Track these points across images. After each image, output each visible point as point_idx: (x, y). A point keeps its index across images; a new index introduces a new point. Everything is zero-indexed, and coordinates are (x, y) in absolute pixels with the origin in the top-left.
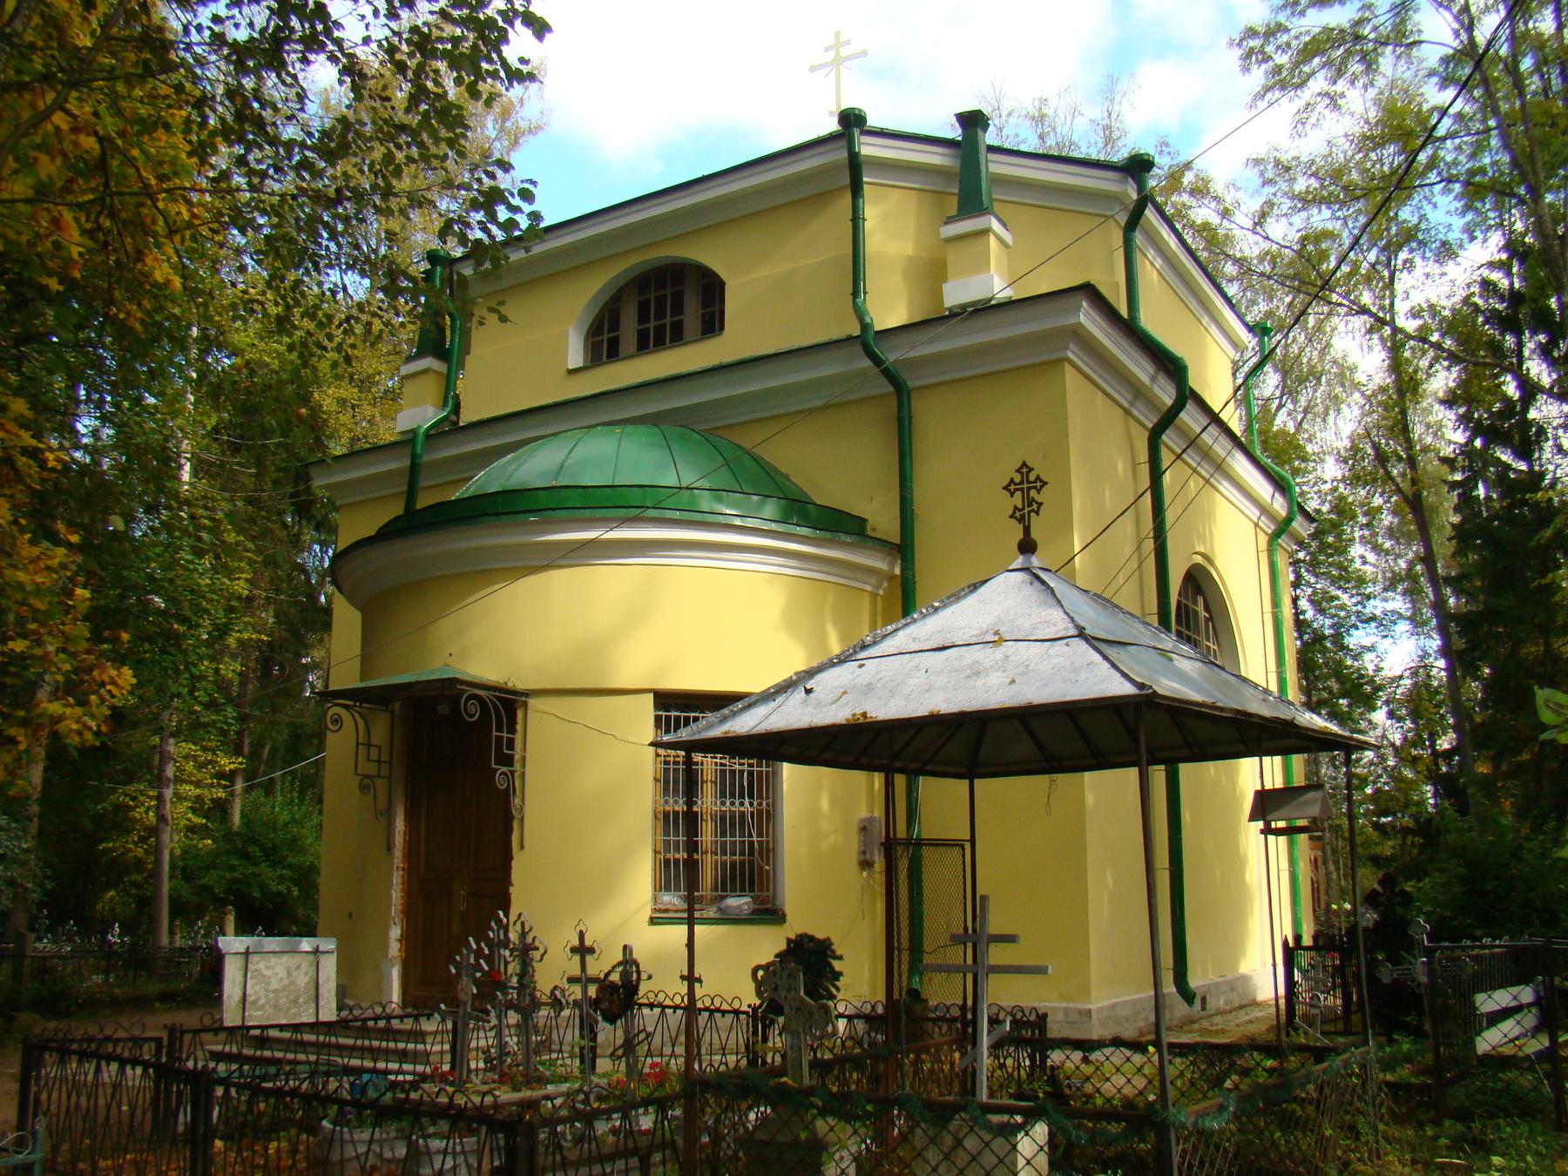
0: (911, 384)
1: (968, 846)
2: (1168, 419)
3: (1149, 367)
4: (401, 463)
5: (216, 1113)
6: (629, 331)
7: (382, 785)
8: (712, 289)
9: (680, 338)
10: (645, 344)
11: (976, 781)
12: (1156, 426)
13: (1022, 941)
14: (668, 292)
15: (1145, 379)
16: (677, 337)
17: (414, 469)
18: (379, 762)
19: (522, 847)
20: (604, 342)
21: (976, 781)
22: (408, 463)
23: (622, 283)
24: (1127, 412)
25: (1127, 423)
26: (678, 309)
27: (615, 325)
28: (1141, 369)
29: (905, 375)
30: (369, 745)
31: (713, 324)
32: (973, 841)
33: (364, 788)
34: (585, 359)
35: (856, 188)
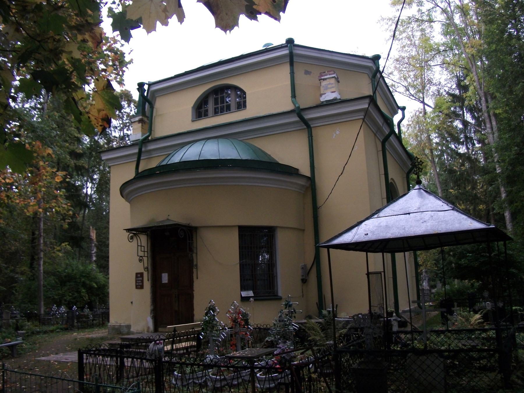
0: (312, 126)
1: (383, 273)
3: (382, 121)
4: (136, 150)
6: (211, 106)
7: (145, 259)
9: (230, 110)
10: (217, 112)
11: (368, 253)
12: (383, 140)
15: (381, 124)
18: (144, 251)
19: (197, 278)
21: (385, 254)
24: (375, 135)
25: (375, 139)
28: (380, 121)
29: (310, 123)
30: (141, 246)
31: (242, 105)
32: (384, 272)
33: (140, 260)
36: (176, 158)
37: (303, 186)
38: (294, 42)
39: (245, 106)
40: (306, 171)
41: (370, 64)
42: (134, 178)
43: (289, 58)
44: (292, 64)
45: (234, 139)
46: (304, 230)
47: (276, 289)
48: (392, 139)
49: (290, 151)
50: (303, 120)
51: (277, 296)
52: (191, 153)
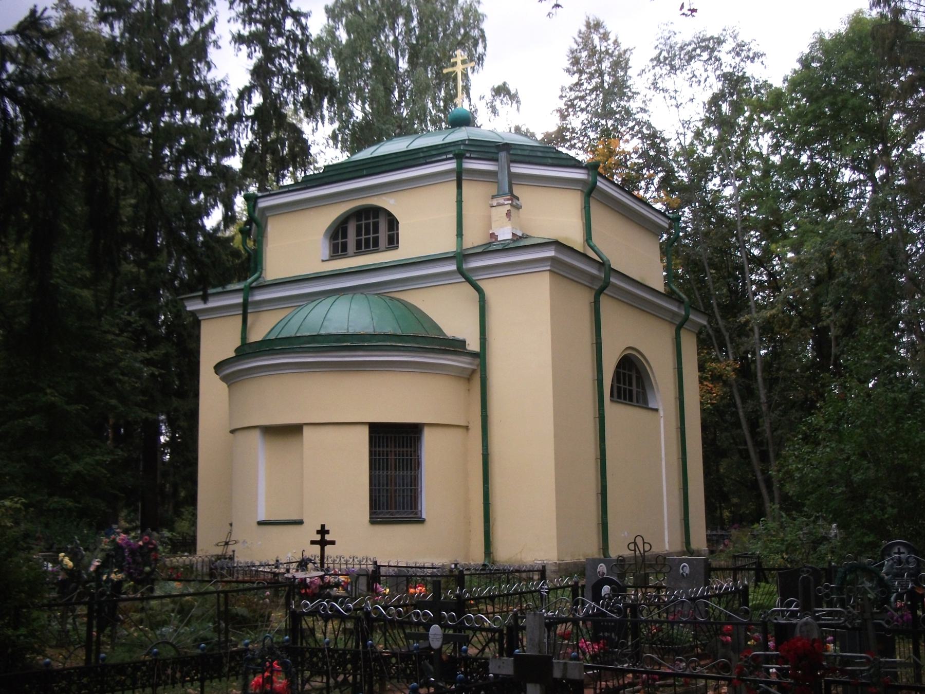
8: (393, 223)
17: (245, 306)
26: (376, 230)
27: (345, 235)
31: (393, 242)
43: (455, 175)
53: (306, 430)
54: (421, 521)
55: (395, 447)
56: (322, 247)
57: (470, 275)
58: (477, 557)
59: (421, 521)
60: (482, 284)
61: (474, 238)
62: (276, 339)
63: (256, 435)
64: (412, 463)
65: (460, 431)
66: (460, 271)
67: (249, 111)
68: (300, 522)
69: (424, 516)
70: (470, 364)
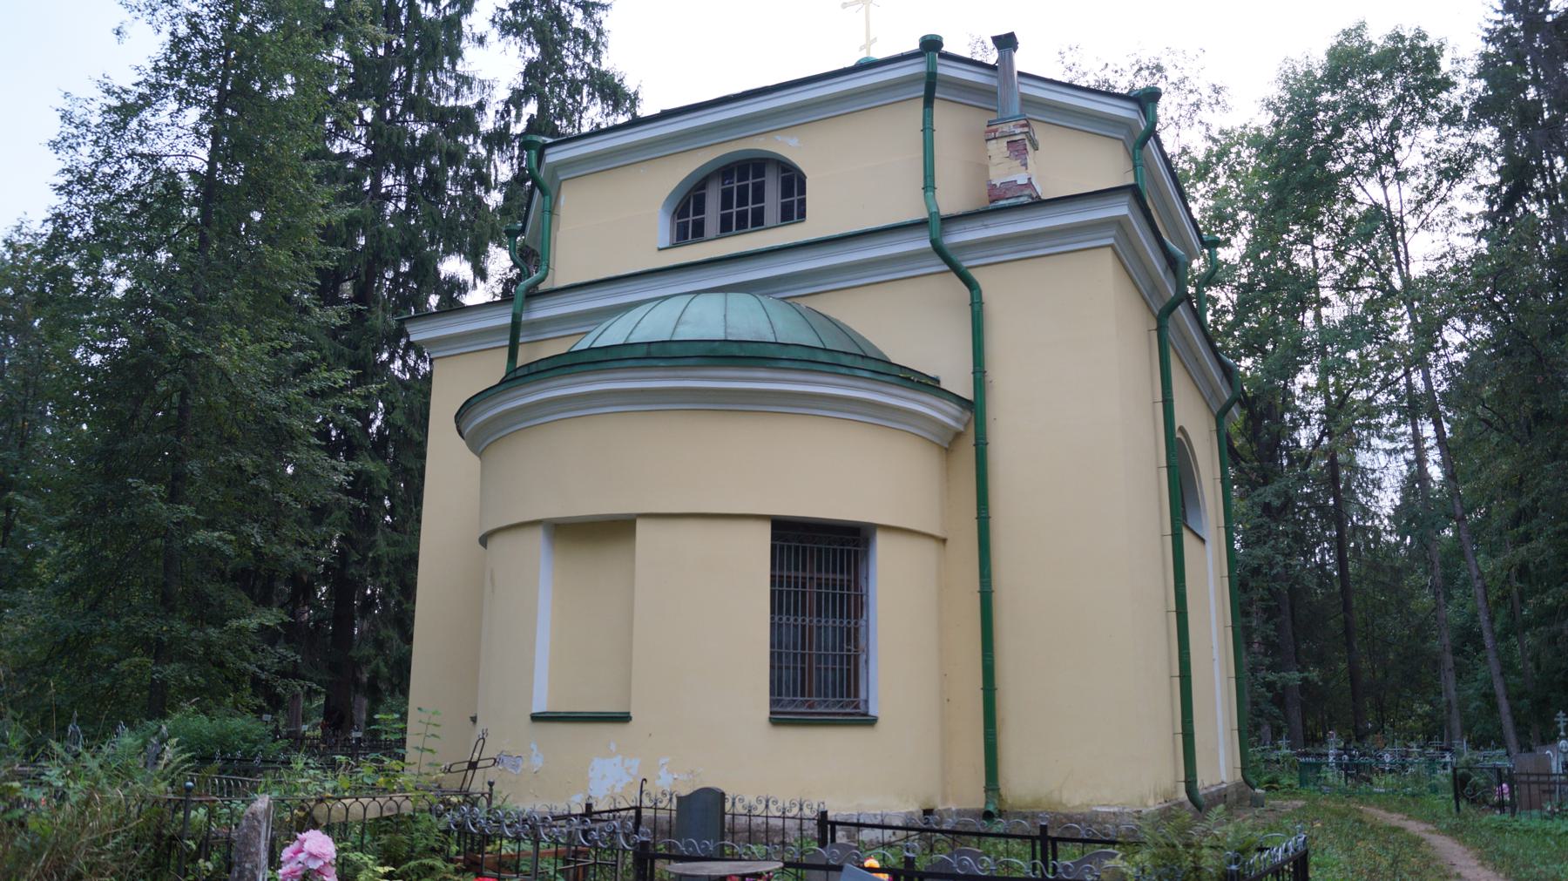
2: (1170, 308)
5: (368, 182)
8: (793, 181)
9: (702, 234)
10: (726, 228)
13: (880, 724)
14: (750, 182)
16: (758, 221)
17: (515, 328)
20: (687, 217)
22: (508, 320)
23: (708, 171)
26: (759, 195)
27: (700, 209)
28: (1157, 264)
31: (793, 212)
34: (668, 238)
35: (929, 101)
36: (614, 333)
37: (944, 426)
38: (941, 45)
39: (802, 216)
40: (959, 381)
41: (1125, 111)
42: (502, 382)
43: (923, 87)
44: (929, 101)
45: (768, 294)
46: (944, 541)
47: (862, 695)
48: (1181, 310)
49: (910, 324)
50: (942, 246)
51: (866, 714)
52: (654, 322)
53: (642, 527)
54: (871, 722)
55: (819, 570)
56: (662, 229)
57: (956, 257)
58: (967, 795)
59: (871, 722)
60: (976, 275)
61: (950, 200)
62: (590, 349)
63: (537, 541)
64: (849, 602)
65: (931, 546)
66: (938, 250)
67: (518, 129)
68: (624, 718)
69: (872, 712)
70: (957, 419)
